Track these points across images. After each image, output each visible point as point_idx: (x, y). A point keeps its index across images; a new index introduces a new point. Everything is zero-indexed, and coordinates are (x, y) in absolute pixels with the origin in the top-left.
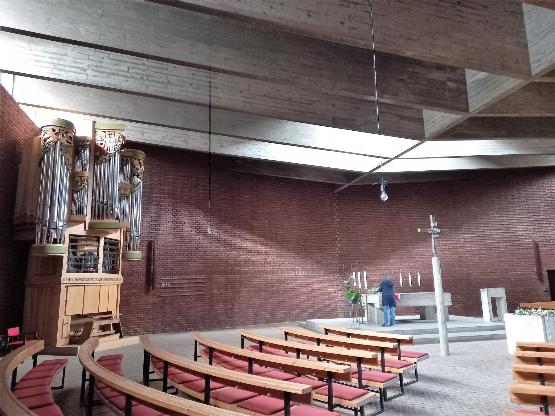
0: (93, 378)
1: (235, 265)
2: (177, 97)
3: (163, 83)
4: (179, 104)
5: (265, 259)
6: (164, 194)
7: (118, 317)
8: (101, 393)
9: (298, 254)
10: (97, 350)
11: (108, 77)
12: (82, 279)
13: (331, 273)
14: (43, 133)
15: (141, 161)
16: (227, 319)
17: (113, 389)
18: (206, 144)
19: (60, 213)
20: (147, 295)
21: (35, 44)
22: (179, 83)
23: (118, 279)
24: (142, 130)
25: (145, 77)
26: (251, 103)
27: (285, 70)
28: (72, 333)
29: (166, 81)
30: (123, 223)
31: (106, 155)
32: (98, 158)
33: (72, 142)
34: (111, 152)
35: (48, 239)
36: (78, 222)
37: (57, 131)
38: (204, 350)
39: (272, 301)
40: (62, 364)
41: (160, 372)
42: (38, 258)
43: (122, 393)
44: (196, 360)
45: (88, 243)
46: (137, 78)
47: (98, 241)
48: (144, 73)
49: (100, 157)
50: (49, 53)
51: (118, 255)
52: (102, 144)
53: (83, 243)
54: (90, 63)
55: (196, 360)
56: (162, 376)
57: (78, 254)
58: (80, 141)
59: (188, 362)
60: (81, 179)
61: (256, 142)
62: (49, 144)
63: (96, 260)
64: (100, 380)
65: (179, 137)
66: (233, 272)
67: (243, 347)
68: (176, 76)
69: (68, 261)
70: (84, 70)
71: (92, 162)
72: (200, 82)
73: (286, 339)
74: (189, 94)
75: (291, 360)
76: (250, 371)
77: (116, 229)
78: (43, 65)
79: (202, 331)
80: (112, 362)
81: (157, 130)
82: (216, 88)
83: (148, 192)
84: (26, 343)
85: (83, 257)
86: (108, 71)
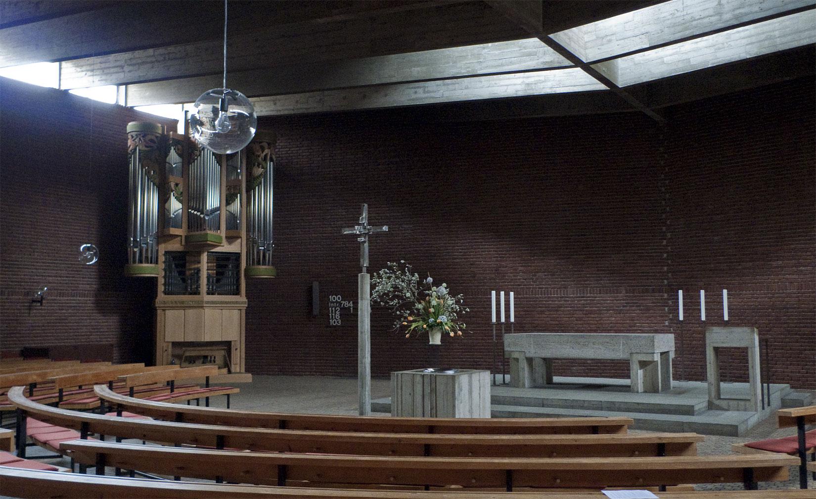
13: (647, 291)
18: (344, 98)
23: (242, 303)
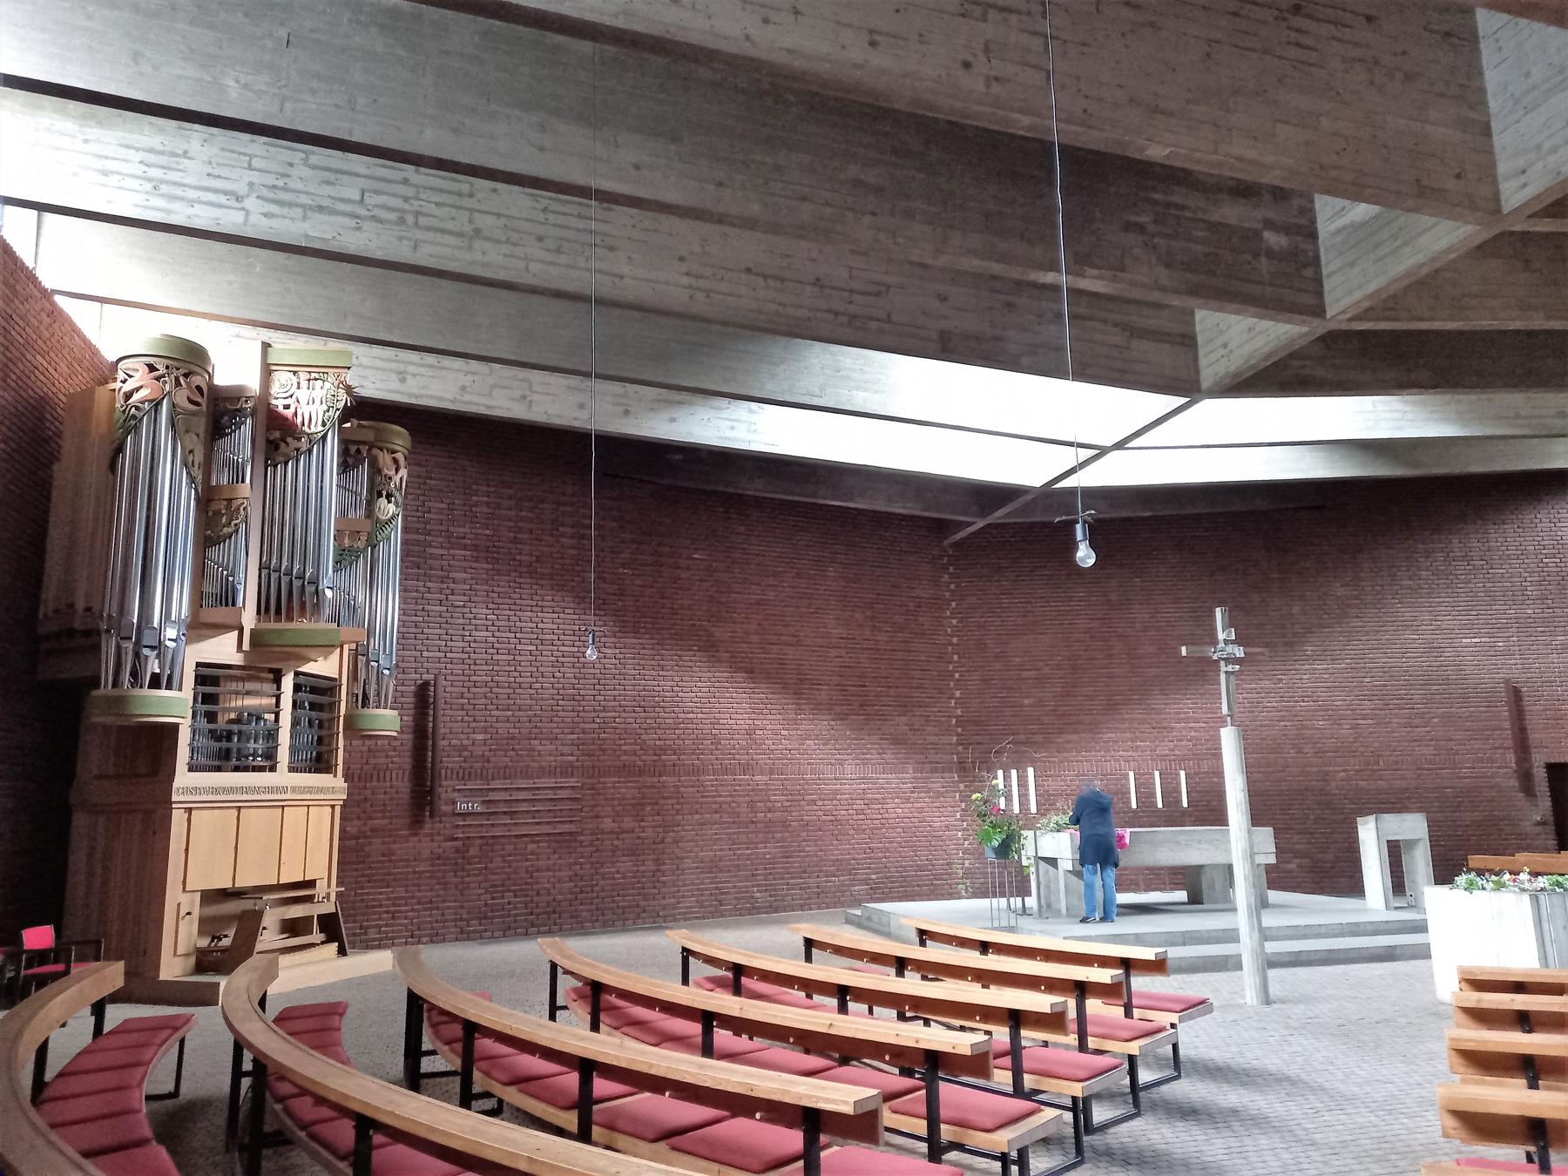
0: (262, 1067)
1: (664, 750)
2: (501, 275)
3: (460, 235)
4: (505, 293)
5: (750, 733)
6: (465, 548)
7: (333, 897)
8: (287, 1110)
9: (843, 717)
10: (273, 990)
11: (305, 218)
12: (231, 790)
13: (934, 771)
14: (121, 375)
15: (400, 456)
16: (643, 903)
17: (321, 1101)
18: (581, 406)
19: (171, 601)
20: (415, 835)
21: (100, 124)
22: (505, 235)
23: (333, 790)
24: (402, 367)
25: (410, 219)
26: (708, 292)
27: (804, 199)
28: (204, 943)
29: (468, 228)
30: (346, 632)
31: (299, 439)
32: (277, 448)
33: (203, 401)
34: (313, 430)
35: (135, 674)
36: (220, 628)
37: (162, 370)
38: (575, 990)
39: (770, 850)
40: (177, 1029)
41: (453, 1051)
42: (106, 729)
43: (345, 1112)
44: (552, 1017)
45: (250, 686)
46: (388, 222)
47: (277, 681)
48: (407, 207)
49: (283, 445)
50: (137, 149)
51: (333, 720)
52: (287, 407)
53: (234, 686)
54: (255, 177)
55: (552, 1017)
56: (457, 1064)
57: (220, 718)
58: (226, 399)
59: (532, 1024)
60: (228, 507)
61: (724, 402)
62: (137, 408)
63: (272, 735)
64: (283, 1075)
65: (505, 388)
66: (659, 770)
67: (685, 981)
68: (499, 215)
69: (193, 739)
70: (239, 199)
71: (260, 458)
72: (565, 233)
73: (808, 958)
74: (534, 267)
75: (821, 1017)
76: (708, 1050)
77: (327, 648)
78: (123, 184)
79: (571, 935)
80: (315, 1023)
81: (443, 368)
82: (611, 249)
83: (418, 543)
84: (74, 971)
85: (235, 728)
86: (304, 199)
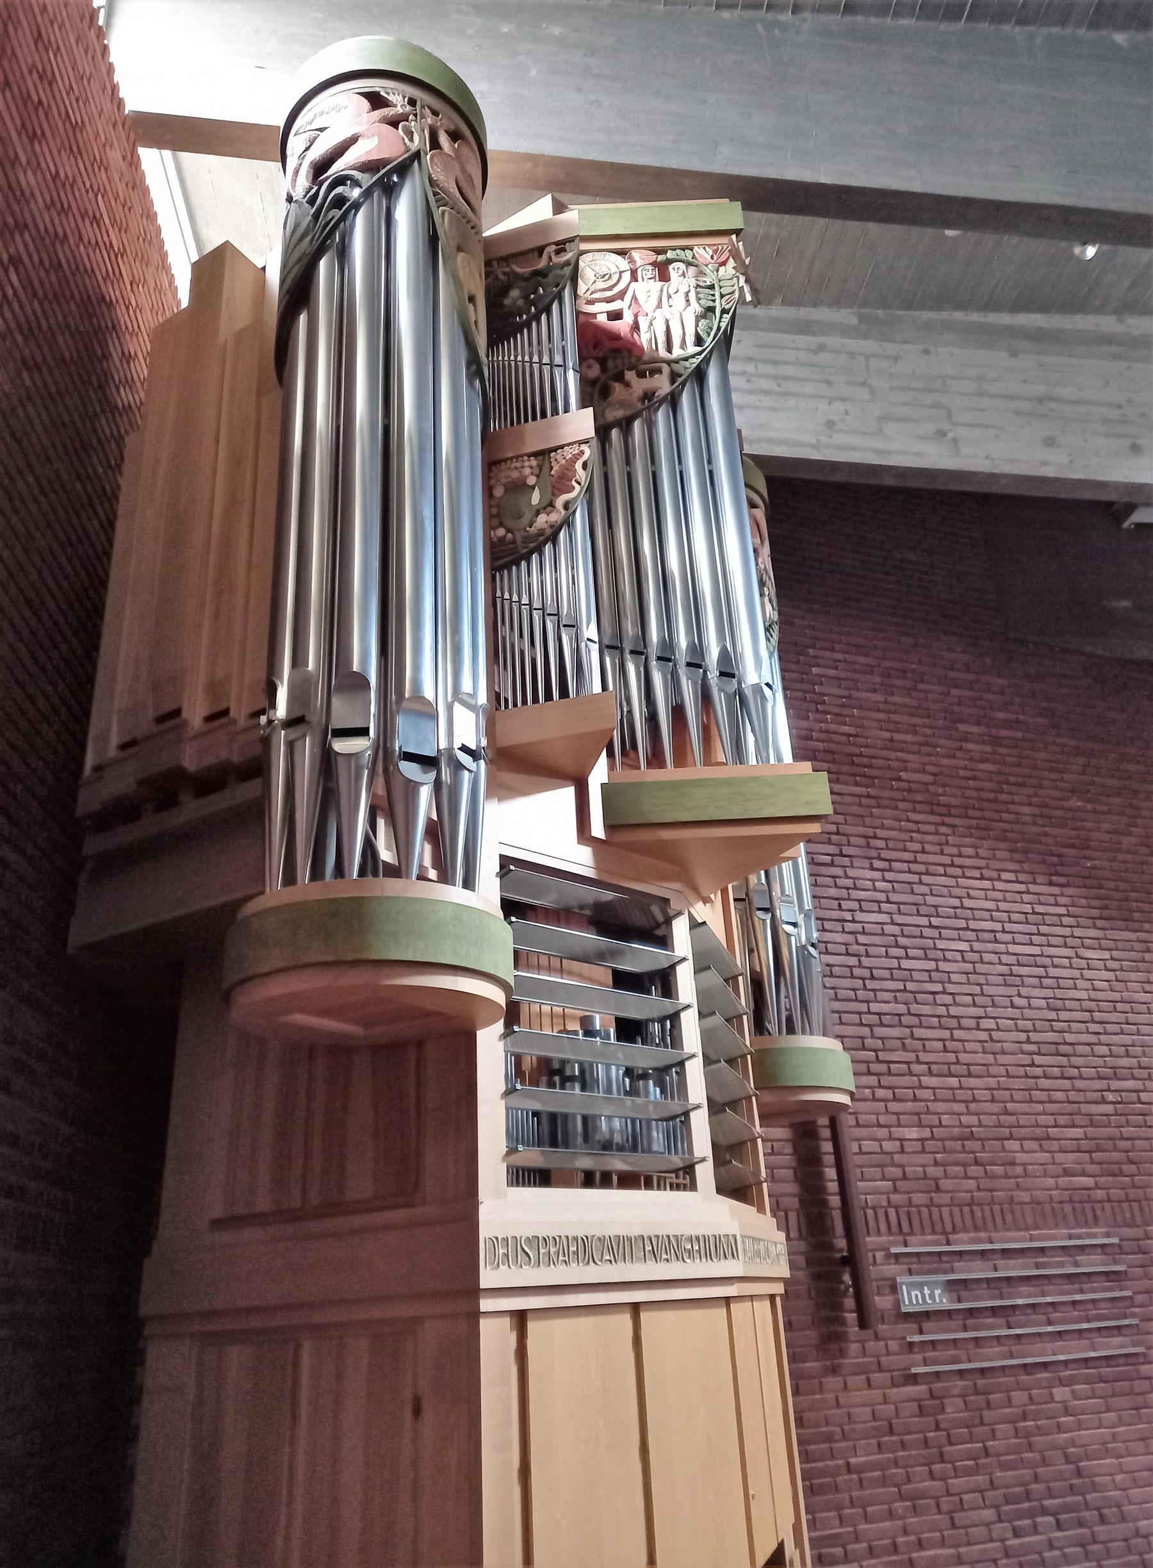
12: (619, 1247)
20: (834, 1370)
34: (677, 352)
37: (399, 104)
49: (617, 387)
52: (616, 316)
81: (787, 394)
